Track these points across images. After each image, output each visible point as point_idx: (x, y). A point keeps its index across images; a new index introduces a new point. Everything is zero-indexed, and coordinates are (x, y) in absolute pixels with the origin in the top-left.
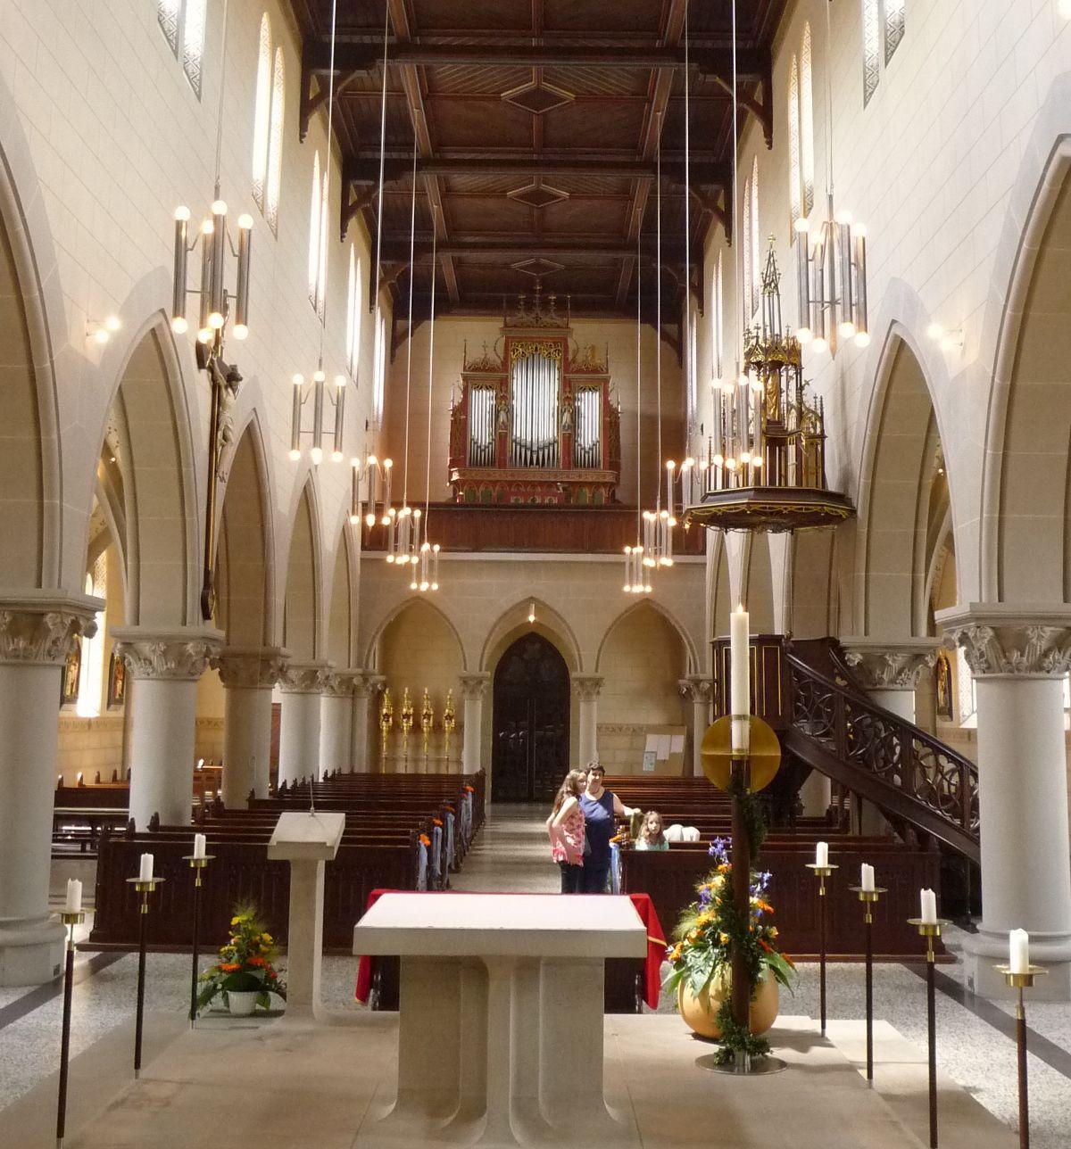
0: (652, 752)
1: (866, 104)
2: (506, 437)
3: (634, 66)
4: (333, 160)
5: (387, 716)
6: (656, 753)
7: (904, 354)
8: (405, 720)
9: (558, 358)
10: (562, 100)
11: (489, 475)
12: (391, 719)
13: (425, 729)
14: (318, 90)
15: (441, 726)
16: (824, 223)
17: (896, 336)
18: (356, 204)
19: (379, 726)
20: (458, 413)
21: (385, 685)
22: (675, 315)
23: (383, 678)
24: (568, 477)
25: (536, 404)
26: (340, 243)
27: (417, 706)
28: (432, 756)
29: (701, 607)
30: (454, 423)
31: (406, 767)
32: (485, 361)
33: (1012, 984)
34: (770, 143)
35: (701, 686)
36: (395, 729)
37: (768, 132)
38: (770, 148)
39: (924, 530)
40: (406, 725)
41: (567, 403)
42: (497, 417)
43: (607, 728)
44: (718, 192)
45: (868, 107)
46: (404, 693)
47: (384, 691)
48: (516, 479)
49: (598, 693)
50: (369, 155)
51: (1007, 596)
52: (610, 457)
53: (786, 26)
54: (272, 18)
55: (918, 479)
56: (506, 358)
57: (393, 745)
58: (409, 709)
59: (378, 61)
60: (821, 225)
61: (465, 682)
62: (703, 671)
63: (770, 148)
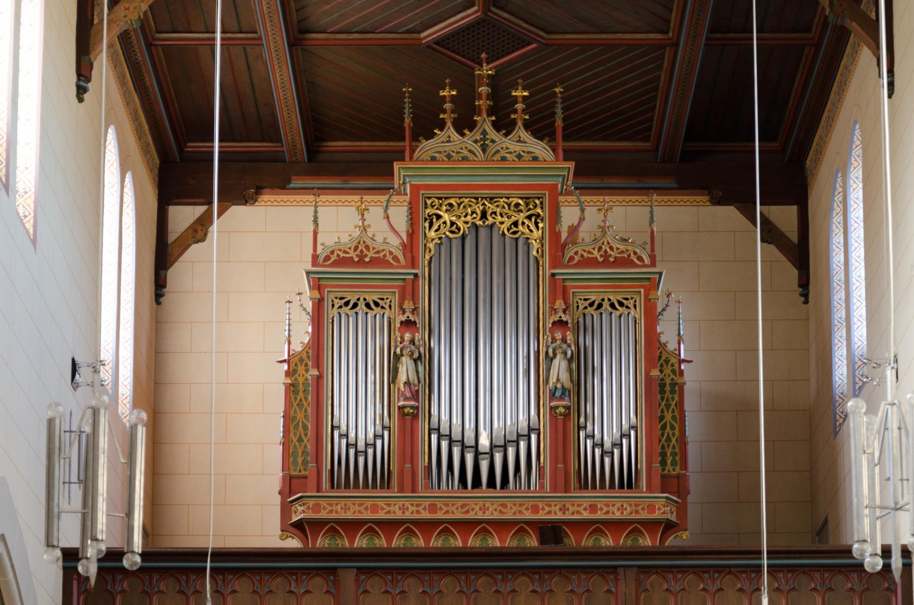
4: (111, 74)
9: (537, 234)
20: (301, 369)
38: (806, 302)
41: (558, 335)
42: (394, 373)
52: (663, 463)
53: (849, 71)
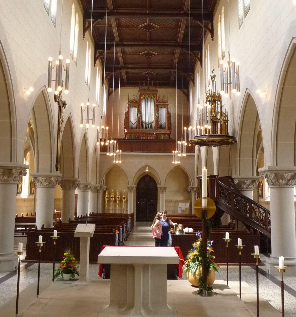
0: (180, 208)
1: (239, 29)
2: (140, 120)
3: (175, 18)
4: (92, 44)
5: (107, 197)
6: (181, 208)
7: (250, 98)
8: (112, 199)
9: (154, 99)
10: (155, 27)
11: (135, 131)
12: (108, 198)
13: (117, 201)
14: (88, 25)
15: (122, 200)
16: (228, 61)
17: (248, 93)
18: (98, 56)
19: (105, 200)
20: (127, 114)
21: (106, 189)
22: (186, 87)
23: (106, 187)
24: (157, 132)
25: (148, 112)
26: (94, 67)
27: (115, 195)
28: (119, 208)
29: (194, 167)
30: (125, 117)
31: (112, 212)
32: (134, 100)
33: (280, 272)
34: (213, 40)
35: (194, 189)
36: (109, 201)
37: (212, 37)
38: (213, 41)
39: (255, 146)
40: (112, 200)
41: (157, 111)
42: (137, 115)
43: (168, 201)
44: (198, 53)
45: (240, 29)
46: (112, 191)
47: (106, 191)
48: (143, 132)
49: (165, 191)
50: (102, 43)
51: (278, 164)
52: (169, 126)
53: (217, 7)
54: (75, 5)
55: (254, 132)
56: (140, 99)
57: (109, 206)
58: (113, 196)
59: (105, 17)
60: (227, 62)
61: (128, 188)
62: (194, 185)
63: (213, 41)
